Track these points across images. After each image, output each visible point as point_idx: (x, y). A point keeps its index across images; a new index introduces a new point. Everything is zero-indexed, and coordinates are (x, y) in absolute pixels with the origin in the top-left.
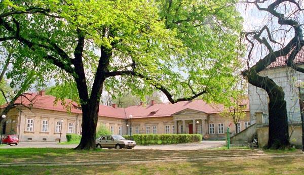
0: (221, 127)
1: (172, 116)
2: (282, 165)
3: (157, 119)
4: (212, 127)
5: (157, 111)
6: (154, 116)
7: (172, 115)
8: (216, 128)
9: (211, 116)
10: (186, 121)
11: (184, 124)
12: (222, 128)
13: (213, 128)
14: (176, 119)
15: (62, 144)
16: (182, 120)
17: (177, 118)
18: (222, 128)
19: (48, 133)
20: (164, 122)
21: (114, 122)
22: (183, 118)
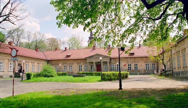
0: (80, 67)
1: (86, 59)
2: (54, 45)
3: (72, 61)
4: (113, 67)
5: (71, 55)
6: (70, 58)
7: (86, 58)
8: (116, 67)
9: (112, 60)
10: (96, 62)
11: (94, 65)
12: (81, 68)
13: (148, 66)
14: (88, 61)
15: (4, 78)
16: (93, 61)
17: (89, 60)
18: (87, 68)
19: (4, 71)
20: (78, 63)
21: (28, 61)
22: (94, 61)
